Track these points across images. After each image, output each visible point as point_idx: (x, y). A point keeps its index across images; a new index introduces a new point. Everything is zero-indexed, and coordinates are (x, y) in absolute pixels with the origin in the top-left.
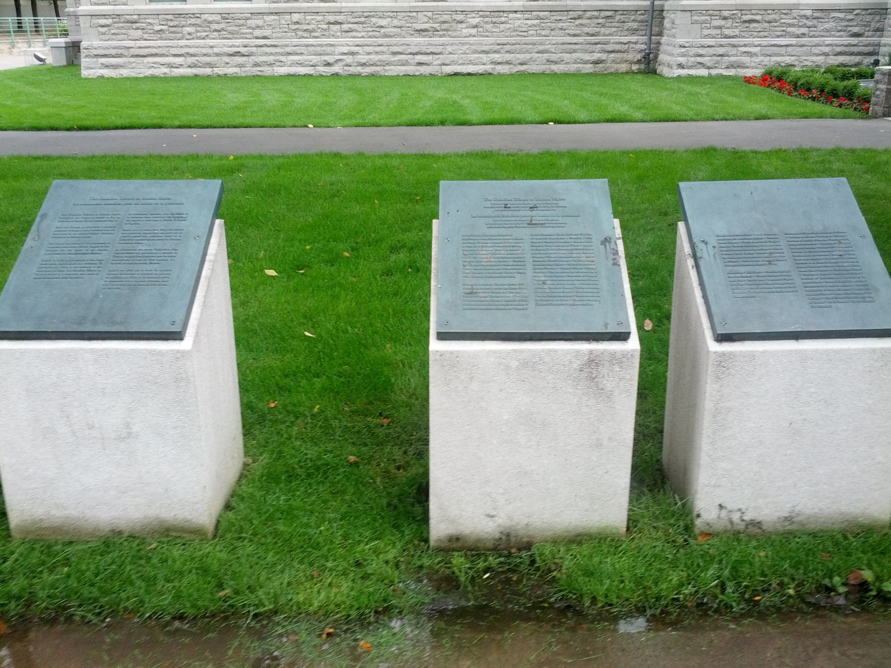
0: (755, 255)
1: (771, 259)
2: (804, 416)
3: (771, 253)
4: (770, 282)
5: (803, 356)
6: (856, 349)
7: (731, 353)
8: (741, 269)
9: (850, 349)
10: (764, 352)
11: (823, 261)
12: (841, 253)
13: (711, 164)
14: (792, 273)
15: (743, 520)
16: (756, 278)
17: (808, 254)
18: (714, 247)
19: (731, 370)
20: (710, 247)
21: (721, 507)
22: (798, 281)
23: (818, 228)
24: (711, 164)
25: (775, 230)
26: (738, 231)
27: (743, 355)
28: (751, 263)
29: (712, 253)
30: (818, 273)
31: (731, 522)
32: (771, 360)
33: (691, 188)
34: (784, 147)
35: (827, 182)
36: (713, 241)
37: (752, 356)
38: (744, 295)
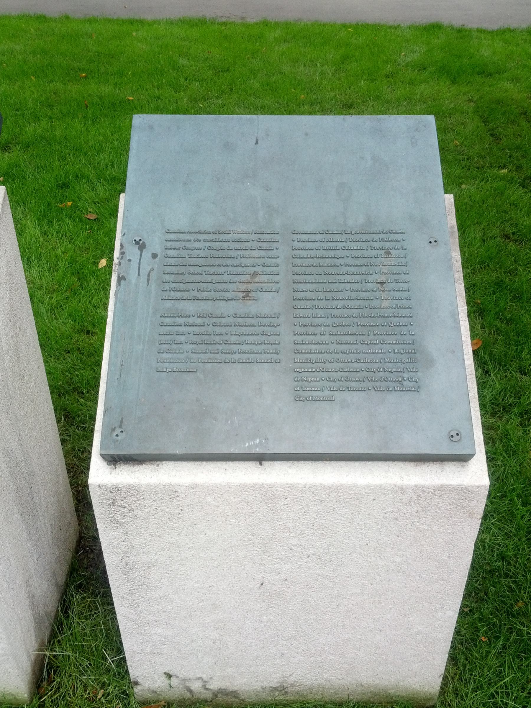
0: (226, 277)
1: (250, 287)
2: (284, 576)
3: (255, 274)
4: (234, 339)
5: (269, 494)
6: (367, 486)
7: (130, 488)
8: (190, 307)
9: (355, 486)
10: (194, 487)
11: (347, 294)
12: (383, 278)
13: (429, 44)
14: (282, 319)
15: (207, 689)
16: (210, 329)
17: (322, 279)
18: (154, 256)
19: (137, 511)
20: (147, 254)
21: (169, 676)
22: (286, 336)
23: (356, 220)
24: (429, 44)
25: (277, 223)
26: (207, 222)
27: (155, 491)
28: (212, 294)
29: (146, 268)
30: (329, 321)
31: (190, 691)
32: (209, 499)
33: (151, 127)
34: (514, 25)
35: (399, 123)
36: (155, 244)
37: (172, 492)
38: (176, 367)
